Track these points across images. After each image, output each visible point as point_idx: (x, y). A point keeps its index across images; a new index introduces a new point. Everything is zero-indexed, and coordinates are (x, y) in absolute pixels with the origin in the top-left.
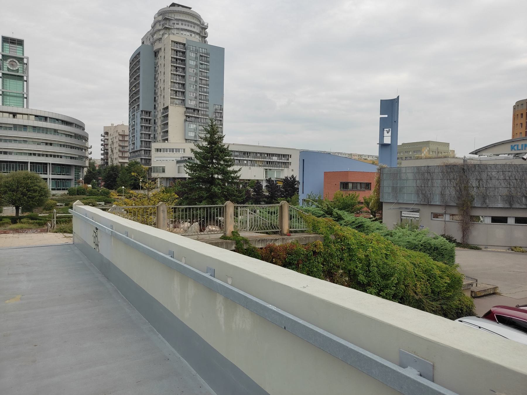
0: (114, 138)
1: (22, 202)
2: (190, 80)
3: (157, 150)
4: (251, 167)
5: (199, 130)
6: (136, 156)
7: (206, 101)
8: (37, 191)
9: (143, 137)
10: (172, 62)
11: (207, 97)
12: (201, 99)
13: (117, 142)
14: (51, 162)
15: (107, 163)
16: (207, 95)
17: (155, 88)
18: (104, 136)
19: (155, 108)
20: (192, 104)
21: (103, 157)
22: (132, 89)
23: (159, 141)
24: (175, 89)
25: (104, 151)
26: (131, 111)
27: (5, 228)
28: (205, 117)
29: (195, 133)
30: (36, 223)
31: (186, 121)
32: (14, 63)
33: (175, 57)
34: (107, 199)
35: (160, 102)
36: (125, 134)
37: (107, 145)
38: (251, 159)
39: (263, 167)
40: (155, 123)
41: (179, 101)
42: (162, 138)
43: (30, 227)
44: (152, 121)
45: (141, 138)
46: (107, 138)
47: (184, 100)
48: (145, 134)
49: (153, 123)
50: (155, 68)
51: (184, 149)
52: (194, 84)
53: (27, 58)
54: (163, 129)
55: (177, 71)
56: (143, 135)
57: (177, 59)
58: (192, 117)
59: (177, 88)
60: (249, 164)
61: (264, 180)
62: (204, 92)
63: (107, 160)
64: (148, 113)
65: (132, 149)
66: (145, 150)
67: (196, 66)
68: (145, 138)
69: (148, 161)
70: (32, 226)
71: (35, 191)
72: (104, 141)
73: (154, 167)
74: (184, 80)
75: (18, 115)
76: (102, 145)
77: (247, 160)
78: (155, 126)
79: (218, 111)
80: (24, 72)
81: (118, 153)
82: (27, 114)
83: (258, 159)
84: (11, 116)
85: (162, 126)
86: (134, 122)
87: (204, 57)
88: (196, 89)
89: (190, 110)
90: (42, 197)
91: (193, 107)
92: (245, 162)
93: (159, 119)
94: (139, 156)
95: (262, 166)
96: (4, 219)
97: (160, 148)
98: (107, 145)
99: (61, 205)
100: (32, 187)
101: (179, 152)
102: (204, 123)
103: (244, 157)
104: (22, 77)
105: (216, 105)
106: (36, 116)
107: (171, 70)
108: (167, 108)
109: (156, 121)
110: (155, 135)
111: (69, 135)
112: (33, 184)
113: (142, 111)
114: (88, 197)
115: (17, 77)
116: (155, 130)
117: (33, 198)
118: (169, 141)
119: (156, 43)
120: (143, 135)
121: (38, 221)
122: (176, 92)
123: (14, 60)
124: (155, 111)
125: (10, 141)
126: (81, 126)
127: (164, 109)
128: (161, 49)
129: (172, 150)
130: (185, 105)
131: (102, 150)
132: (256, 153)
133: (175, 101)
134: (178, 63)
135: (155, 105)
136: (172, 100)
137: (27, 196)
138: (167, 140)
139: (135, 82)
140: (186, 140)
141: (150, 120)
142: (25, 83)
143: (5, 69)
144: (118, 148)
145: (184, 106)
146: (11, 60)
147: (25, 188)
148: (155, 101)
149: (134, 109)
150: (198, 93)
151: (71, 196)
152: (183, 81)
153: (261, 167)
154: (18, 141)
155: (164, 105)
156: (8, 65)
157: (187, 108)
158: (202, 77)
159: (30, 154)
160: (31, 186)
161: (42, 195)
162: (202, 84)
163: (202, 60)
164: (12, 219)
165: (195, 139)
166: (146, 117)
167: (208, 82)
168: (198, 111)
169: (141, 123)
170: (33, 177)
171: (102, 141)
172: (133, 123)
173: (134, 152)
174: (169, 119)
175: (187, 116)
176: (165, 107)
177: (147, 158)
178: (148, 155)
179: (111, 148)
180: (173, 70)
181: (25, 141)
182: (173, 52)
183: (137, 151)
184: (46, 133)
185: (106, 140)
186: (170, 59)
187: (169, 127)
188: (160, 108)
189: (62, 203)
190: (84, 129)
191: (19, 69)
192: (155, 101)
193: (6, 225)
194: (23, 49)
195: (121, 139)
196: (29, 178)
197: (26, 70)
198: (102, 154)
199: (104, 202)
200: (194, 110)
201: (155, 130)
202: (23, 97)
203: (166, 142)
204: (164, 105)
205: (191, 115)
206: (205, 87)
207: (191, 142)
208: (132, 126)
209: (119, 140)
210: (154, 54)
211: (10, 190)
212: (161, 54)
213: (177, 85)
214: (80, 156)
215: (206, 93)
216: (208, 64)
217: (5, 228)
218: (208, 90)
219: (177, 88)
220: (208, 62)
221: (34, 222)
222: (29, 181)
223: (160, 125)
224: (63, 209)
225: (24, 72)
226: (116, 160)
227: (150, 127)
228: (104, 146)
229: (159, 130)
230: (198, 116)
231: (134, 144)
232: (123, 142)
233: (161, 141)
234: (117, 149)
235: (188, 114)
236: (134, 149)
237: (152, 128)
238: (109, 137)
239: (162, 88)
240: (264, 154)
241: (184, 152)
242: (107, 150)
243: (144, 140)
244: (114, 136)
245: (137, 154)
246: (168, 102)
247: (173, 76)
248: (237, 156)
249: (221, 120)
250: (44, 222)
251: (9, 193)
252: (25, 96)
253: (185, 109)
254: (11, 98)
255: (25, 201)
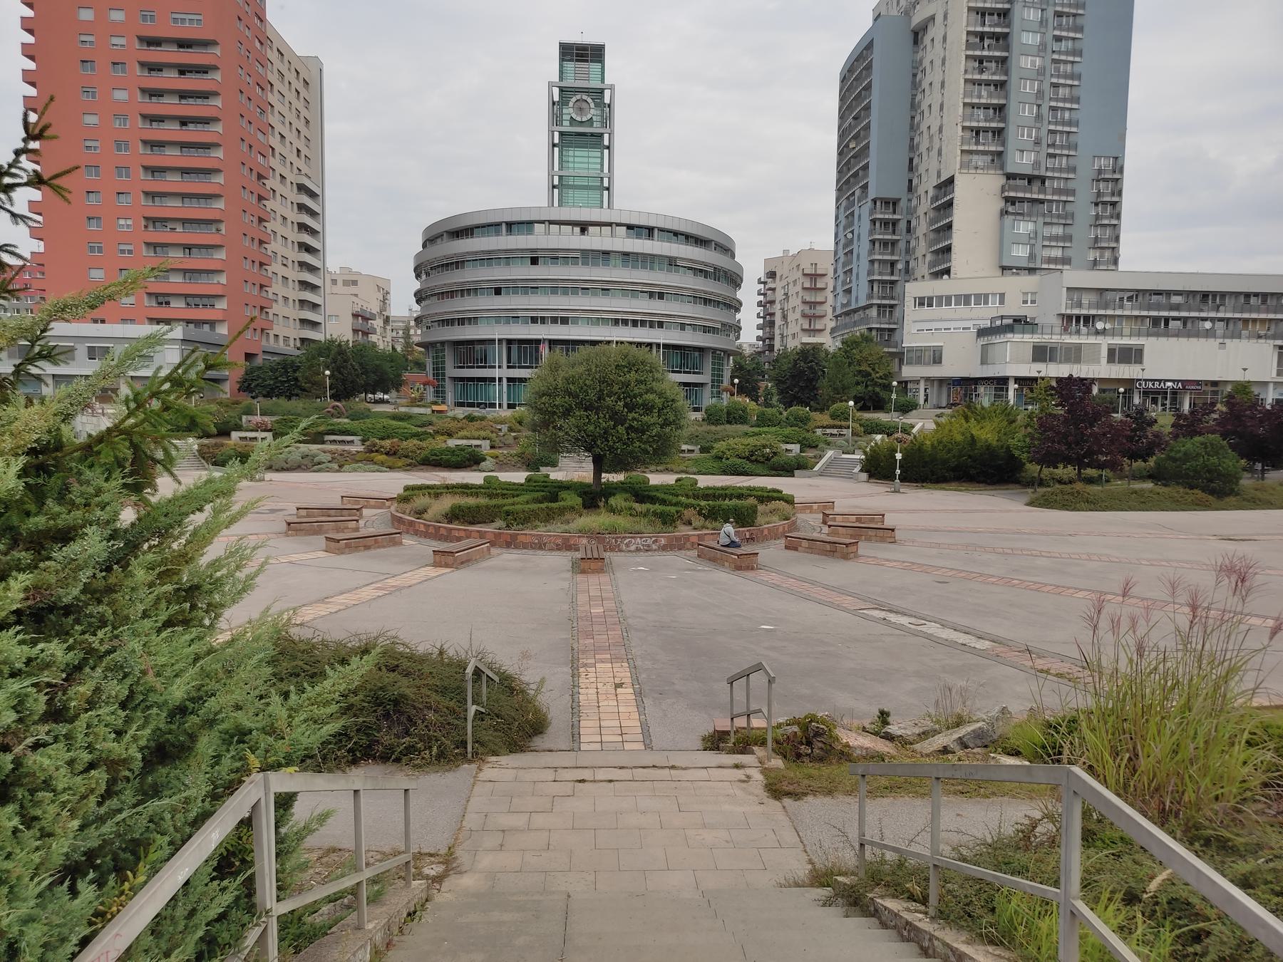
0: (791, 286)
1: (611, 443)
2: (1023, 89)
3: (921, 302)
4: (1227, 341)
5: (1044, 238)
6: (855, 324)
7: (1069, 148)
8: (653, 407)
9: (876, 271)
10: (969, 46)
11: (1072, 138)
12: (1053, 145)
13: (797, 293)
14: (662, 341)
15: (771, 348)
16: (1074, 129)
17: (913, 134)
18: (765, 283)
19: (910, 189)
20: (1022, 161)
21: (760, 333)
22: (847, 146)
23: (919, 278)
24: (975, 124)
25: (764, 318)
26: (844, 204)
27: (567, 527)
28: (1064, 198)
29: (1032, 246)
30: (655, 514)
31: (1004, 213)
32: (584, 105)
33: (979, 29)
34: (808, 435)
35: (927, 170)
36: (819, 272)
37: (772, 302)
38: (1229, 315)
39: (1271, 342)
40: (909, 230)
41: (985, 157)
42: (929, 269)
43: (637, 528)
44: (902, 226)
45: (870, 273)
46: (772, 286)
47: (1000, 154)
48: (880, 261)
49: (905, 230)
50: (915, 75)
51: (1002, 296)
52: (1033, 100)
53: (612, 88)
54: (938, 241)
55: (982, 72)
56: (876, 265)
57: (982, 36)
58: (1022, 200)
59: (980, 120)
60: (1219, 332)
61: (1271, 386)
62: (1064, 123)
63: (772, 339)
64: (892, 204)
65: (843, 305)
66: (879, 306)
67: (1042, 48)
68: (880, 274)
69: (890, 334)
70: (642, 524)
71: (648, 409)
72: (765, 295)
73: (910, 350)
74: (1003, 93)
75: (591, 229)
76: (760, 304)
77: (1212, 320)
78: (909, 237)
79: (1107, 176)
80: (604, 125)
81: (801, 321)
82: (610, 224)
83: (1254, 316)
84: (577, 229)
85: (932, 236)
86: (852, 232)
87: (1068, 15)
88: (1039, 117)
89: (1019, 182)
90: (668, 430)
91: (1029, 171)
92: (1208, 325)
93: (922, 216)
94: (861, 322)
95: (1266, 337)
96: (563, 494)
97: (931, 295)
98: (772, 302)
99: (691, 451)
100: (641, 395)
101: (986, 303)
102: (1059, 216)
103: (1201, 310)
104: (601, 135)
105: (1100, 157)
106: (630, 227)
107: (966, 71)
108: (951, 181)
109: (913, 223)
110: (907, 263)
111: (700, 271)
112: (643, 387)
113: (874, 201)
114: (756, 430)
115: (589, 139)
116: (908, 251)
117: (643, 432)
118: (952, 275)
119: (918, 7)
120: (876, 265)
121: (658, 508)
122: (977, 133)
123: (585, 97)
124: (910, 196)
125: (575, 291)
126: (726, 248)
127: (938, 187)
128: (932, 18)
129: (965, 299)
130: (1002, 168)
131: (758, 316)
132: (1247, 295)
133: (975, 157)
134: (986, 46)
135: (910, 181)
136: (966, 158)
137: (627, 425)
138: (947, 271)
139: (856, 126)
140: (1004, 268)
141: (895, 223)
142: (606, 152)
143: (566, 123)
144: (801, 307)
145: (1001, 172)
146: (578, 97)
147: (620, 400)
148: (911, 168)
149: (851, 199)
150: (1046, 127)
151: (713, 428)
152: (999, 98)
153: (1263, 341)
154: (590, 291)
155: (939, 176)
156: (571, 110)
157: (1010, 177)
158: (1058, 77)
159: (616, 322)
160: (637, 391)
161: (666, 423)
162: (1057, 100)
163: (1060, 27)
164: (585, 493)
165: (1032, 265)
166: (887, 217)
167: (1075, 92)
168: (1043, 182)
169: (871, 232)
170: (642, 363)
171: (759, 294)
172: (850, 236)
173: (847, 314)
174: (955, 211)
175: (1007, 199)
176: (943, 179)
177: (887, 326)
178: (886, 320)
179: (782, 309)
180: (970, 70)
181: (606, 289)
182: (973, 15)
183: (855, 311)
184: (652, 268)
185: (769, 292)
186: (964, 37)
187: (954, 235)
188: (927, 185)
189: (692, 443)
190: (733, 256)
191: (594, 118)
192: (911, 168)
193: (568, 516)
194: (603, 68)
195: (807, 285)
196: (631, 366)
197: (607, 120)
198: (759, 327)
199: (798, 446)
200: (1030, 179)
201: (908, 251)
202: (602, 187)
203: (945, 277)
204: (939, 176)
205: (1020, 195)
206: (1068, 105)
207: (1018, 274)
208: (845, 246)
209: (804, 289)
210: (910, 38)
211: (580, 405)
212: (935, 32)
213: (981, 113)
214: (723, 325)
215: (1070, 123)
216: (1078, 36)
217: (567, 527)
218: (1075, 115)
219: (980, 120)
220: (1079, 29)
221: (648, 510)
222: (632, 376)
223: (925, 234)
224: (696, 460)
225: (604, 125)
226: (793, 338)
227: (894, 243)
228: (764, 306)
229: (922, 248)
230: (1041, 197)
231: (848, 291)
232: (813, 292)
233: (927, 276)
234: (798, 311)
235: (1012, 194)
236: (849, 303)
237: (902, 245)
238: (778, 284)
239: (934, 129)
240: (1139, 319)
241: (1002, 302)
242: (772, 314)
243: (879, 278)
244: (791, 280)
245: (856, 317)
246: (952, 163)
247: (970, 87)
248: (1177, 307)
249: (1114, 204)
250: (677, 512)
251: (577, 413)
252: (606, 184)
253: (1003, 180)
254: (578, 193)
255: (620, 440)
